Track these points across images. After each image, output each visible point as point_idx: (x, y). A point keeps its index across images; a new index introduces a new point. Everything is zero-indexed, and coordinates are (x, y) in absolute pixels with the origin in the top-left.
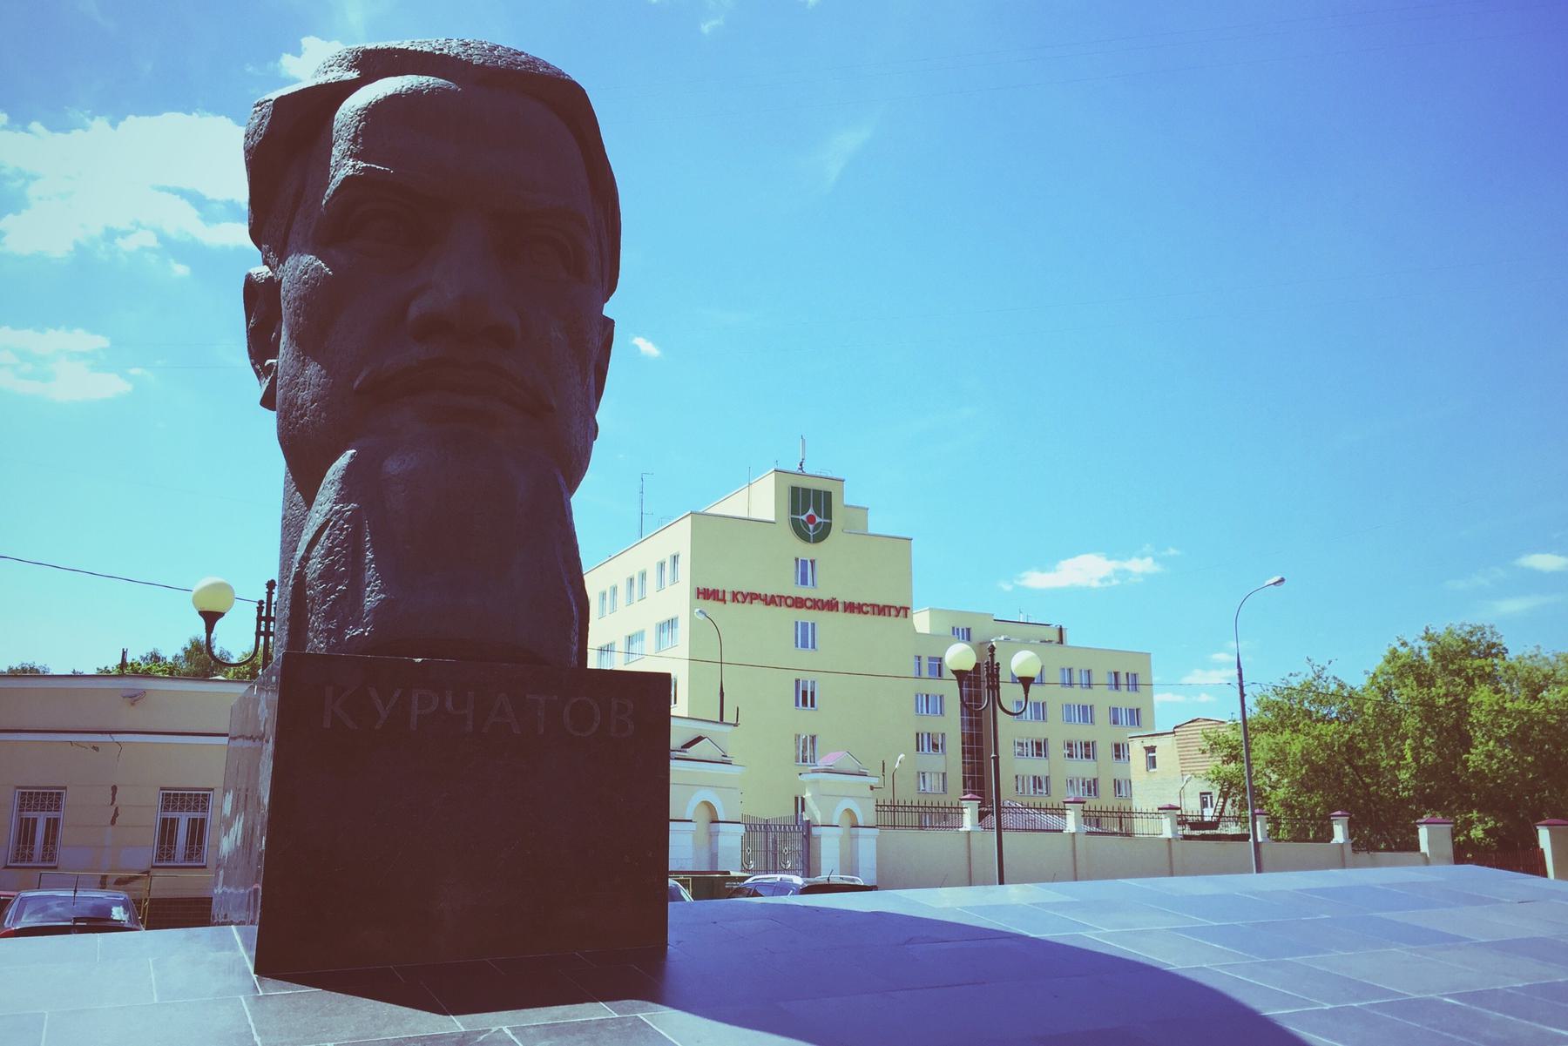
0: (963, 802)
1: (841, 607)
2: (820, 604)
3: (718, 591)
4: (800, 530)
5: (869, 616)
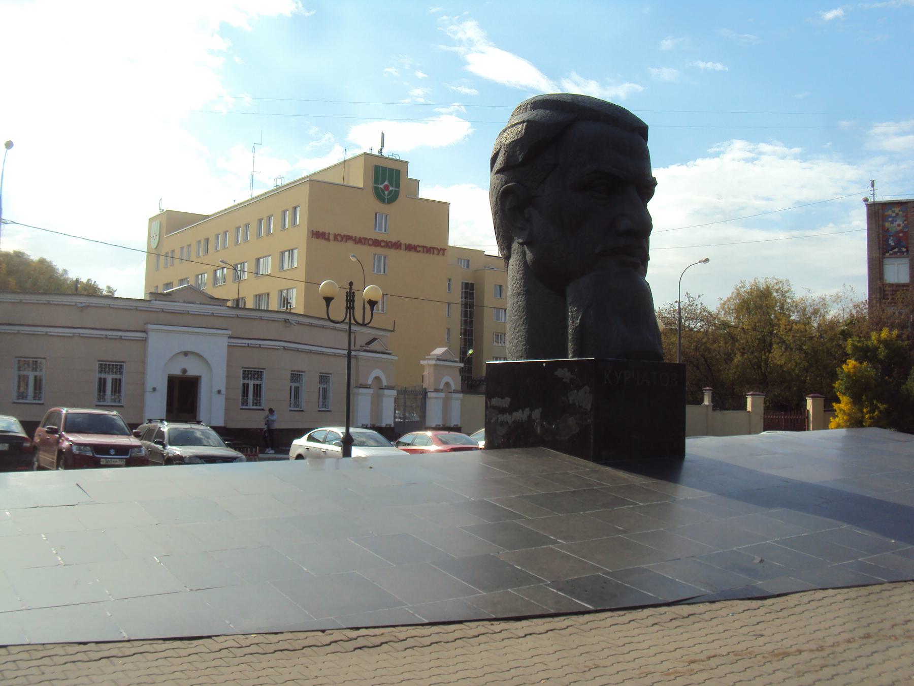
1: (403, 247)
2: (390, 244)
3: (325, 233)
4: (380, 195)
5: (420, 254)
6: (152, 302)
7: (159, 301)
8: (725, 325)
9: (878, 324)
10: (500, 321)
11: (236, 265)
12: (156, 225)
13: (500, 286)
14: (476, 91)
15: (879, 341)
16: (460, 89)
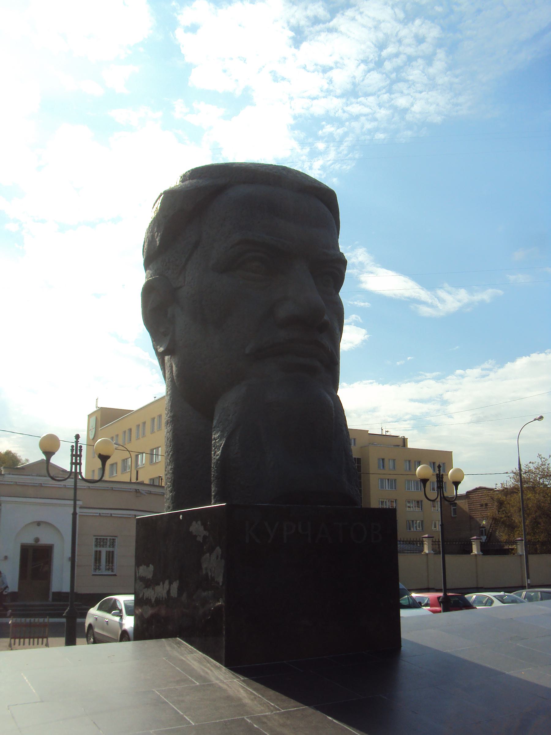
0: (424, 539)
6: (6, 476)
7: (13, 474)
10: (384, 489)
11: (152, 450)
12: (93, 419)
14: (369, 304)
16: (356, 303)
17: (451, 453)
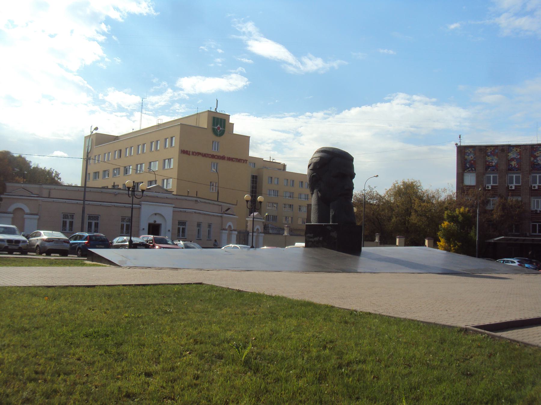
2: (220, 157)
4: (215, 132)
8: (388, 202)
9: (459, 204)
13: (271, 178)
15: (460, 213)
16: (242, 59)
17: (248, 138)
